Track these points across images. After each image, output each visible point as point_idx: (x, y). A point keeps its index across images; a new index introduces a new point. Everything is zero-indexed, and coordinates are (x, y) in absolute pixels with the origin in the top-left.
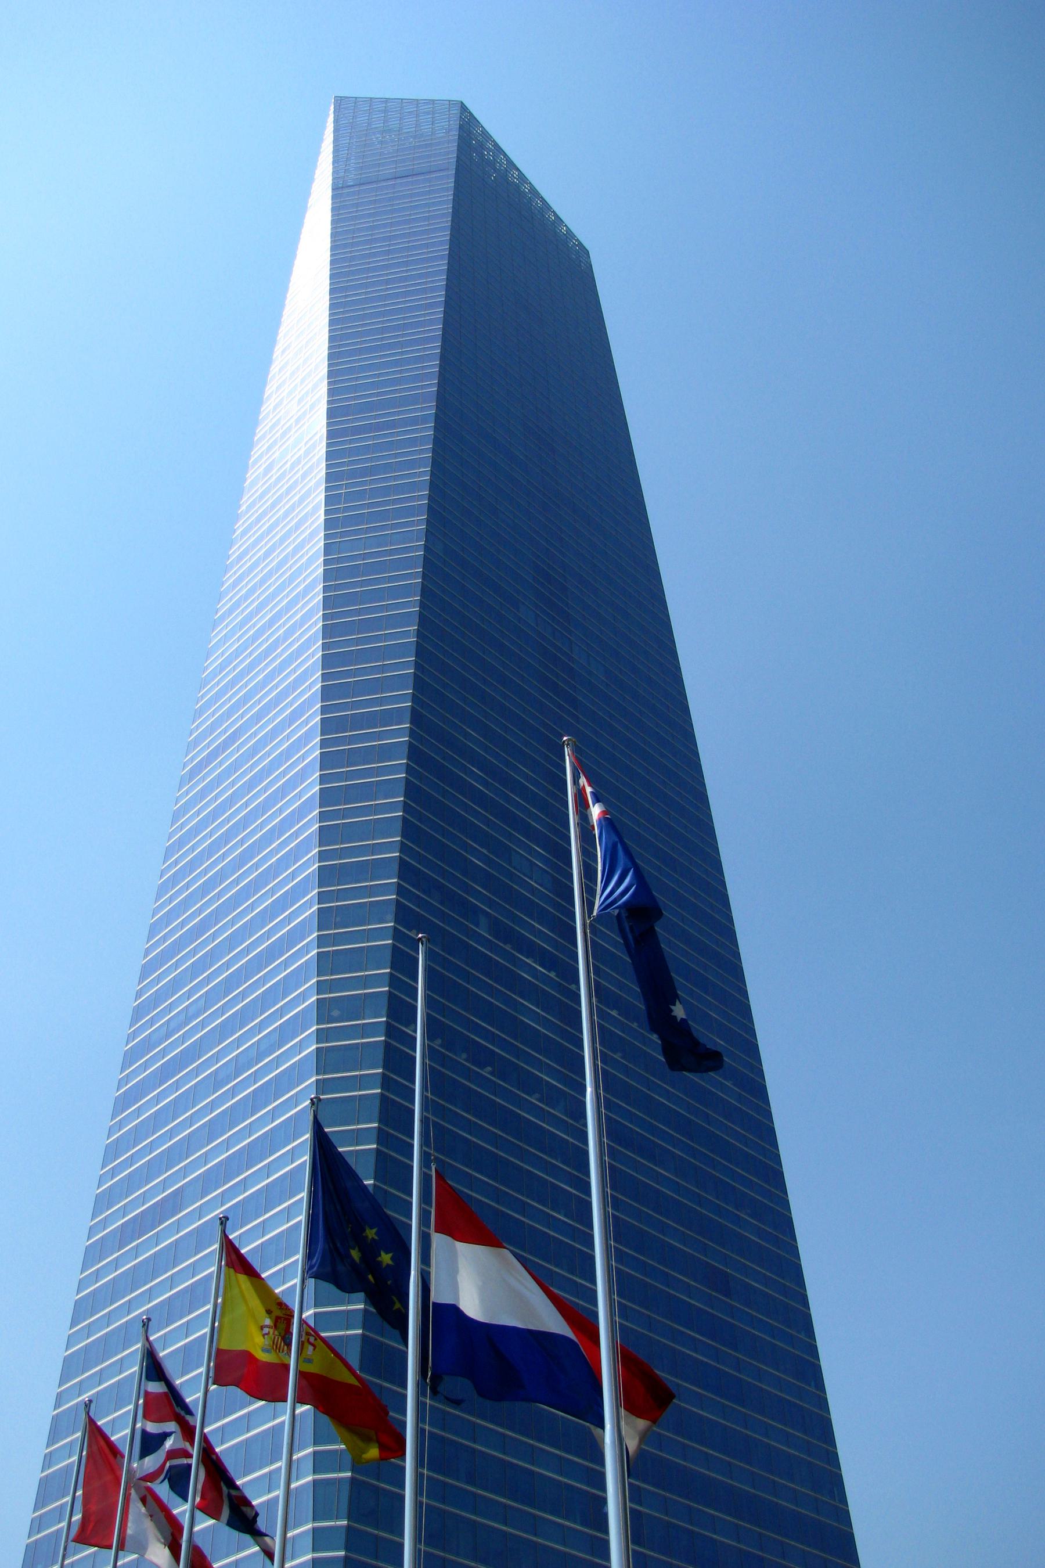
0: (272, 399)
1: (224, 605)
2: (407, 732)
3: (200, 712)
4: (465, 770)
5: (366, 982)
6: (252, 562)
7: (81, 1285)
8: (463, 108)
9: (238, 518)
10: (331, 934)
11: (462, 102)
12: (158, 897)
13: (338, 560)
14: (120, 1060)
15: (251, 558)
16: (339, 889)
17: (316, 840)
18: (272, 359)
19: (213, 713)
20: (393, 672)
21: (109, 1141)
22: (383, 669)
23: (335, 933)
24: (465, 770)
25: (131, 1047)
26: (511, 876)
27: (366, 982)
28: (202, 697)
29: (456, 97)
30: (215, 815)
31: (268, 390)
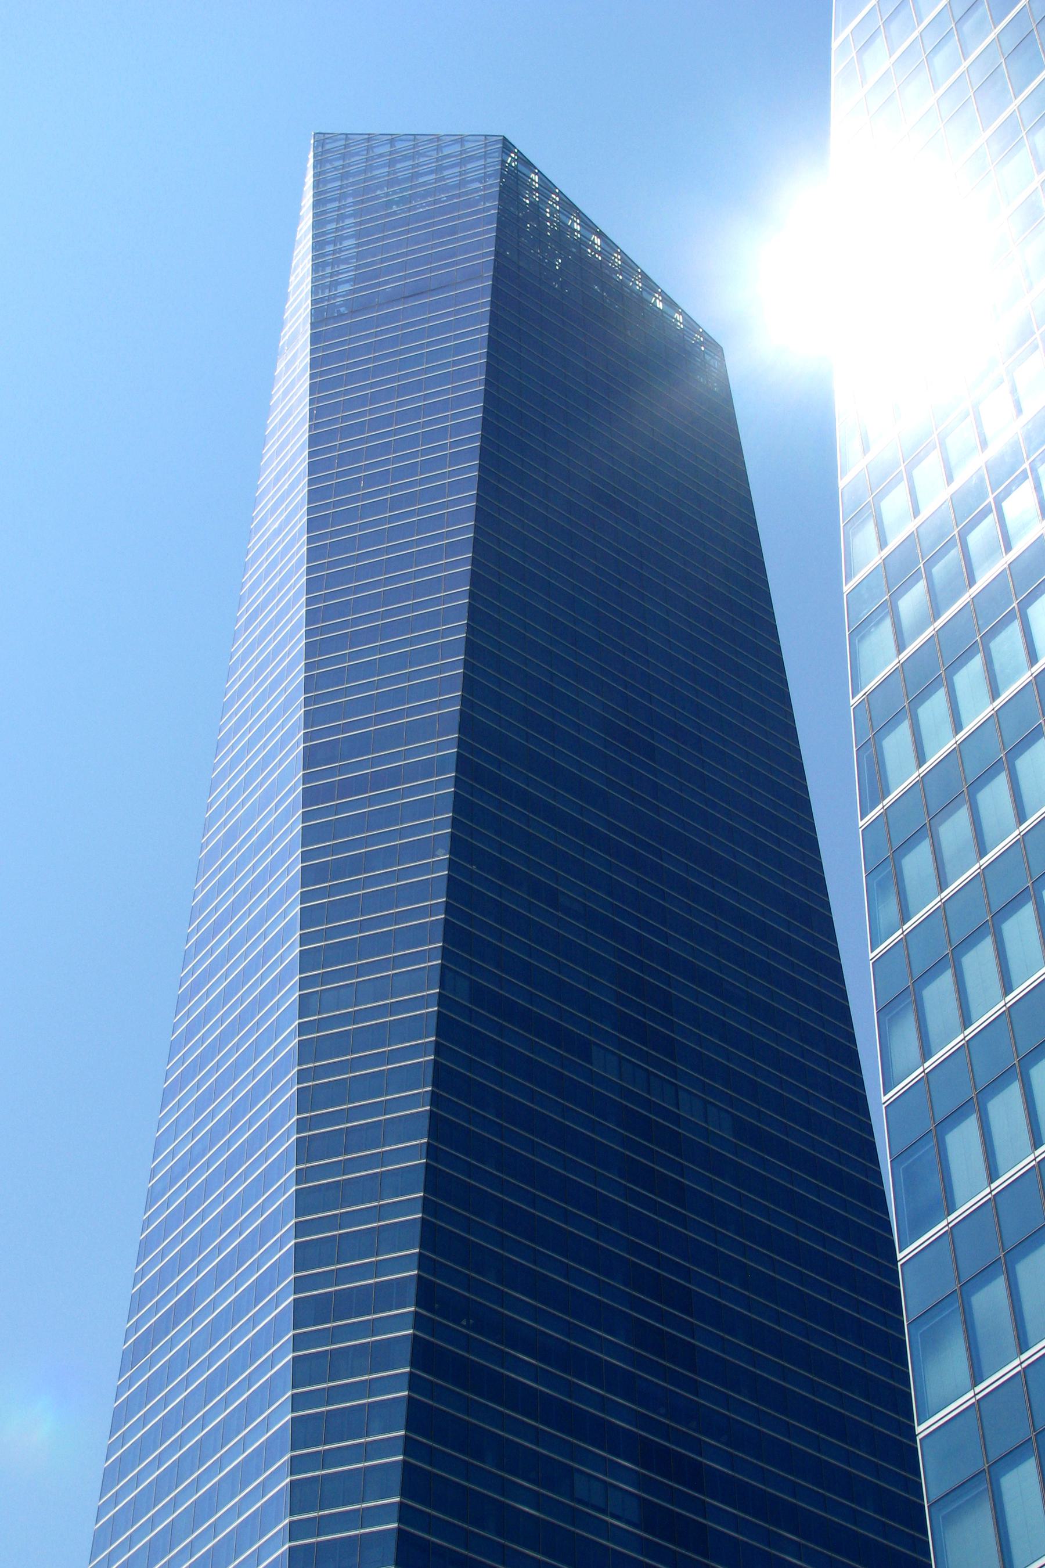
0: (299, 270)
1: (239, 647)
2: (419, 1205)
3: (207, 825)
4: (502, 1358)
5: (364, 1517)
6: (282, 414)
7: (110, 1451)
8: (507, 146)
9: (255, 502)
10: (355, 965)
11: (505, 139)
12: (149, 1205)
13: (319, 1025)
14: (127, 1305)
15: (267, 558)
16: (353, 1058)
17: (285, 1502)
18: (294, 240)
19: (229, 785)
20: (422, 578)
21: (135, 1290)
22: (380, 1213)
23: (329, 1388)
24: (502, 1358)
25: (146, 1236)
26: (574, 1516)
27: (364, 1517)
28: (207, 842)
29: (497, 128)
30: (164, 1429)
31: (297, 256)
